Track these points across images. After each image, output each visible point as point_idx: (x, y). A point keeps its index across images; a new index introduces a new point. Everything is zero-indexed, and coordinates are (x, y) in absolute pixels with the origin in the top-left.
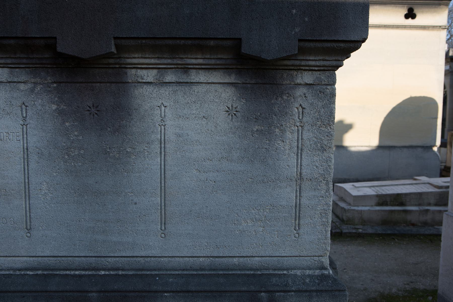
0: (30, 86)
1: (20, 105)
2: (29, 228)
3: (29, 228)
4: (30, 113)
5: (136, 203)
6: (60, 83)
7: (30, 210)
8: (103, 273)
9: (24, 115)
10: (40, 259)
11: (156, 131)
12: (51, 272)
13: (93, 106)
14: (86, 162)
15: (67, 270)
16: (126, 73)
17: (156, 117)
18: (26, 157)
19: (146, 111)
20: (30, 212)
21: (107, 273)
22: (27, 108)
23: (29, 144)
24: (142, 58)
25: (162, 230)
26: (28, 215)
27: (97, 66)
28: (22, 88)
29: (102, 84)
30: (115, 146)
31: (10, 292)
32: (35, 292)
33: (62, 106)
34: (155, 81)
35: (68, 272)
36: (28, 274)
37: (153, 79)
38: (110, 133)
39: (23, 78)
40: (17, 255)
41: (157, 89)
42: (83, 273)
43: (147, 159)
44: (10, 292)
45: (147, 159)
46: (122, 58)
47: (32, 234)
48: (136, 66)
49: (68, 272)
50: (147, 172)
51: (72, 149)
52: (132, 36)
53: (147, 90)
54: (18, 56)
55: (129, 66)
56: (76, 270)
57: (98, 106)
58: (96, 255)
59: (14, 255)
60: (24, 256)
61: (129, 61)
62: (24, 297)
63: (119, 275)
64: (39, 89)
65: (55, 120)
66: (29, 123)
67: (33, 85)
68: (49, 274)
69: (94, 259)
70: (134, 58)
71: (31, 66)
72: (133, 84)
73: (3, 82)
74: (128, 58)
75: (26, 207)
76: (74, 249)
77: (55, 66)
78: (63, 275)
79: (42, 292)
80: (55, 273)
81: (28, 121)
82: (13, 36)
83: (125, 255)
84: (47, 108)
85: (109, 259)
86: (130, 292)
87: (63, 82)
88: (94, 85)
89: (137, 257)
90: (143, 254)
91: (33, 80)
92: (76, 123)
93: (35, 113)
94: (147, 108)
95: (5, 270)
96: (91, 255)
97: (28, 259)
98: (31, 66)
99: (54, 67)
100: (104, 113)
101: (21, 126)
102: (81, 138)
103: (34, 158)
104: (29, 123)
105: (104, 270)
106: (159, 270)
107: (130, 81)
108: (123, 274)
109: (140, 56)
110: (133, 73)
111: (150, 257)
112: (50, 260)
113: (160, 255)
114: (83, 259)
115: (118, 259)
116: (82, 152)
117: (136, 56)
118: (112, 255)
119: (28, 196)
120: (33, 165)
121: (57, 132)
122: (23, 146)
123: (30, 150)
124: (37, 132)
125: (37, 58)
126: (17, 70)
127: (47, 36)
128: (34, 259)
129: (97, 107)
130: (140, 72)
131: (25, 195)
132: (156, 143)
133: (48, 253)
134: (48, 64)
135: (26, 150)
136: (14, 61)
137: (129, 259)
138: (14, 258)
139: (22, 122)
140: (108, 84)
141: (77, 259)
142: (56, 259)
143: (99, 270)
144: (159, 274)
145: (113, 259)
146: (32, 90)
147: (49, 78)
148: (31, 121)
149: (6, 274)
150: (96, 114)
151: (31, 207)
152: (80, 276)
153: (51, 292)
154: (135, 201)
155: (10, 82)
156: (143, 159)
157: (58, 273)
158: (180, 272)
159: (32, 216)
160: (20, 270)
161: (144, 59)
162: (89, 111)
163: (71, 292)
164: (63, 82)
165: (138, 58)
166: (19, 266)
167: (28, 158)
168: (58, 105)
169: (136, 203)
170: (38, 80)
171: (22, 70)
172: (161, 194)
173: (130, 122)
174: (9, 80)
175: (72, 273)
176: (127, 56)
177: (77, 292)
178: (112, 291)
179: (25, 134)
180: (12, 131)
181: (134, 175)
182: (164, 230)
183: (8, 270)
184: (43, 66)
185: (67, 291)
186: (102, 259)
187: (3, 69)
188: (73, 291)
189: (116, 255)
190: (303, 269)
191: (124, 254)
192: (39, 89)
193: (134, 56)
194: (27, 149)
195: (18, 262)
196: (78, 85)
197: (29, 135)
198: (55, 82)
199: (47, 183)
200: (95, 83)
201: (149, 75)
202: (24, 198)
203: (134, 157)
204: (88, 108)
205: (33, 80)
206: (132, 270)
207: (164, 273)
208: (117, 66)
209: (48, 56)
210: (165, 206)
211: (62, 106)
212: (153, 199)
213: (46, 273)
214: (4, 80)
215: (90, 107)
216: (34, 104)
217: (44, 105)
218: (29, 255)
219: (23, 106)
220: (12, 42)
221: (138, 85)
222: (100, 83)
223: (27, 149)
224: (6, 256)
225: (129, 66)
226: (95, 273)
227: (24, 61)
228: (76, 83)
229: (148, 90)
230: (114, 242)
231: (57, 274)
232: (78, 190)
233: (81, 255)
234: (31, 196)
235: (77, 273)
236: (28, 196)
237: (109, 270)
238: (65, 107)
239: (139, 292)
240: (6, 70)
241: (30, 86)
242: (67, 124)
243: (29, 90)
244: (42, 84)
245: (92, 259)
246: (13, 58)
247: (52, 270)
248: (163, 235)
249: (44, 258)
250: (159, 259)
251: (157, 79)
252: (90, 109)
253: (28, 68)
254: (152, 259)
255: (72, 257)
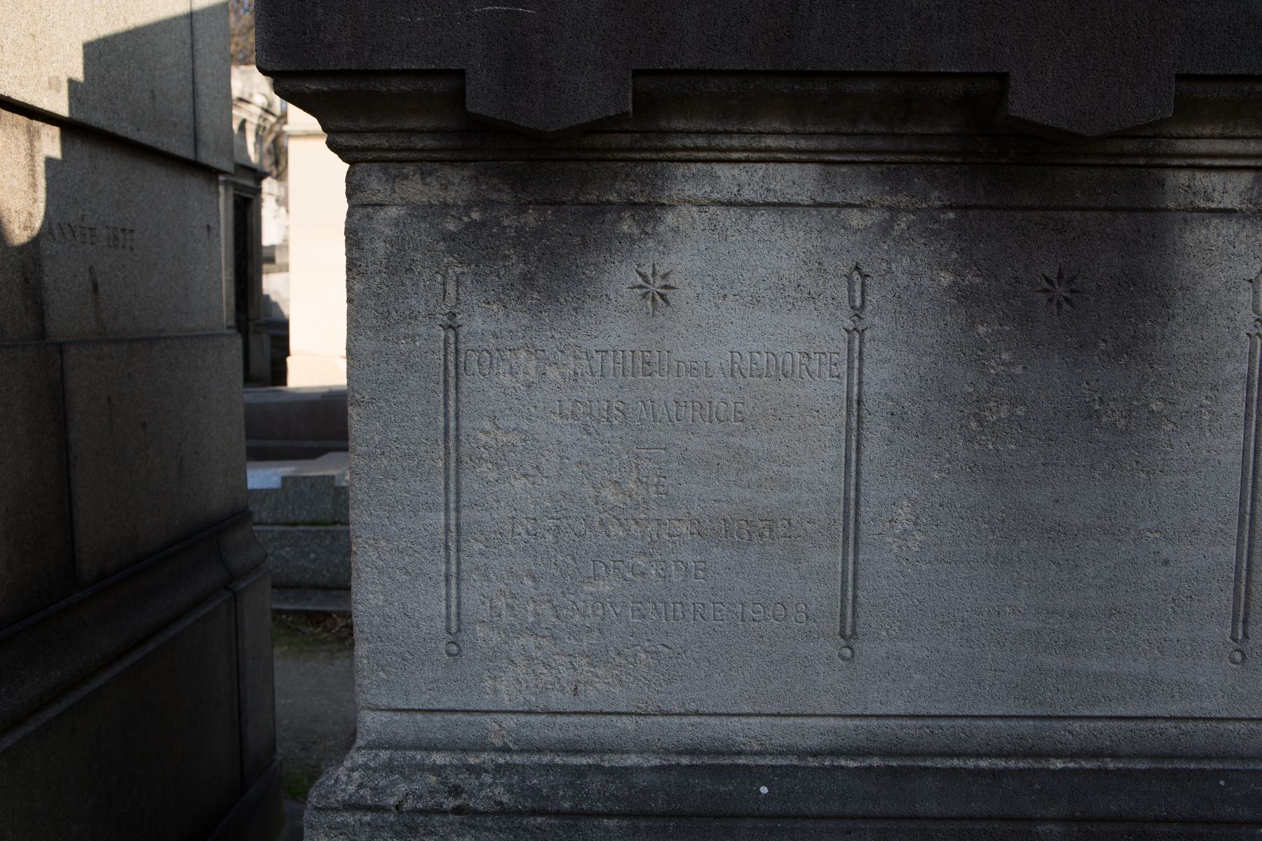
0: (876, 216)
1: (846, 271)
2: (848, 632)
3: (848, 632)
4: (874, 297)
5: (1166, 563)
6: (967, 208)
7: (854, 580)
8: (1059, 764)
9: (858, 303)
10: (874, 722)
11: (1238, 351)
12: (909, 763)
13: (1060, 277)
14: (1032, 441)
15: (952, 755)
16: (1161, 184)
17: (1243, 312)
18: (854, 425)
19: (1214, 293)
20: (855, 586)
21: (1071, 765)
22: (868, 281)
23: (865, 388)
24: (1222, 137)
25: (1235, 640)
26: (850, 594)
27: (1083, 161)
28: (854, 223)
29: (1087, 215)
30: (1116, 394)
31: (806, 817)
32: (877, 818)
33: (969, 277)
34: (1244, 207)
35: (956, 762)
36: (842, 767)
37: (1238, 199)
38: (1106, 358)
39: (860, 193)
40: (810, 711)
41: (1249, 230)
42: (1002, 764)
43: (1208, 434)
44: (806, 817)
45: (1208, 434)
46: (1165, 137)
47: (857, 652)
48: (1197, 161)
49: (956, 762)
50: (1204, 470)
51: (992, 404)
52: (1235, 71)
53: (1217, 233)
54: (861, 127)
55: (1176, 162)
56: (978, 755)
57: (1075, 277)
58: (1039, 713)
59: (800, 710)
60: (829, 715)
61: (1183, 146)
62: (849, 833)
63: (1107, 771)
64: (903, 225)
65: (948, 318)
66: (872, 326)
67: (887, 215)
68: (906, 767)
69: (1031, 723)
70: (1197, 137)
71: (888, 158)
72: (1180, 216)
73: (799, 205)
74: (1182, 138)
75: (844, 573)
76: (975, 694)
77: (958, 160)
78: (945, 769)
79: (902, 818)
80: (922, 764)
81: (868, 318)
82: (883, 69)
83: (1125, 714)
84: (926, 282)
85: (1076, 725)
86: (1156, 821)
87: (976, 207)
88: (1066, 215)
89: (1155, 718)
90: (1175, 709)
91: (888, 200)
92: (1007, 328)
93: (890, 296)
94: (1216, 284)
95: (772, 754)
96: (1023, 712)
97: (841, 722)
98: (888, 158)
99: (955, 164)
100: (1092, 299)
101: (846, 335)
102: (1018, 370)
103: (877, 428)
104: (872, 326)
105: (1059, 755)
106: (1222, 757)
107: (1171, 205)
108: (1119, 769)
109: (1219, 131)
110: (1181, 181)
111: (1195, 719)
112: (902, 727)
113: (1225, 714)
114: (999, 723)
115: (1100, 724)
116: (1021, 411)
117: (1207, 131)
118: (1086, 713)
119: (852, 537)
120: (874, 449)
121: (950, 351)
122: (849, 392)
123: (869, 404)
124: (892, 352)
125: (917, 135)
126: (844, 169)
127: (982, 70)
128: (857, 722)
129: (1071, 280)
130: (1203, 180)
131: (846, 538)
132: (1238, 388)
133: (899, 706)
134: (940, 154)
135: (856, 405)
136: (847, 143)
137: (1132, 724)
138: (799, 720)
139: (848, 324)
140: (1106, 215)
141: (982, 723)
142: (920, 723)
143: (1047, 755)
144: (1224, 770)
145: (1085, 723)
146: (885, 230)
147: (936, 194)
148: (876, 321)
149: (781, 767)
150: (1067, 300)
151: (861, 572)
152: (994, 774)
153: (928, 818)
154: (1165, 555)
155: (818, 205)
156: (1196, 432)
157: (928, 763)
158: (707, 760)
159: (861, 599)
160: (815, 754)
161: (1225, 141)
162: (1046, 291)
163: (982, 819)
164: (976, 207)
165: (1211, 137)
166: (813, 742)
167: (859, 428)
168: (957, 273)
169: (1166, 563)
170: (903, 199)
171: (859, 169)
172: (1240, 534)
173: (1165, 326)
174: (818, 199)
175: (971, 763)
176: (1179, 130)
177: (1002, 819)
178: (1104, 820)
179: (857, 357)
180: (818, 350)
181: (1168, 479)
182: (1242, 642)
183: (781, 753)
184: (925, 158)
185: (971, 818)
186: (1056, 724)
187: (804, 166)
188: (990, 818)
189: (1098, 714)
190: (464, 750)
191: (1121, 711)
192: (903, 225)
193: (1199, 130)
194: (859, 402)
195: (812, 733)
196: (1019, 215)
197: (867, 360)
198: (951, 207)
199: (914, 503)
200: (1065, 209)
201: (1229, 189)
202: (840, 544)
203: (1171, 426)
204: (1045, 284)
205: (888, 200)
206: (1140, 756)
207: (1239, 765)
208: (1142, 161)
209: (949, 130)
210: (1249, 570)
211: (969, 277)
212: (1218, 549)
213: (895, 764)
214: (804, 199)
215: (1048, 281)
216: (890, 271)
217: (916, 271)
218: (844, 712)
219: (856, 276)
220: (872, 86)
221: (1193, 218)
222: (1083, 209)
223: (859, 402)
224: (779, 715)
225: (1176, 162)
226: (1036, 765)
227: (877, 143)
228: (1012, 208)
229: (1224, 232)
230: (1095, 674)
231: (926, 768)
232: (1003, 521)
233: (994, 713)
234: (864, 538)
235: (984, 763)
236: (852, 537)
237: (1073, 756)
238: (978, 280)
239: (1182, 821)
240: (812, 170)
241: (876, 216)
242: (982, 330)
243: (875, 229)
244: (913, 213)
245: (1024, 723)
246: (846, 134)
247: (909, 755)
248: (1238, 656)
249: (886, 722)
250: (1222, 725)
251: (1250, 201)
252: (1049, 287)
253: (873, 163)
254: (1201, 724)
255: (966, 717)
